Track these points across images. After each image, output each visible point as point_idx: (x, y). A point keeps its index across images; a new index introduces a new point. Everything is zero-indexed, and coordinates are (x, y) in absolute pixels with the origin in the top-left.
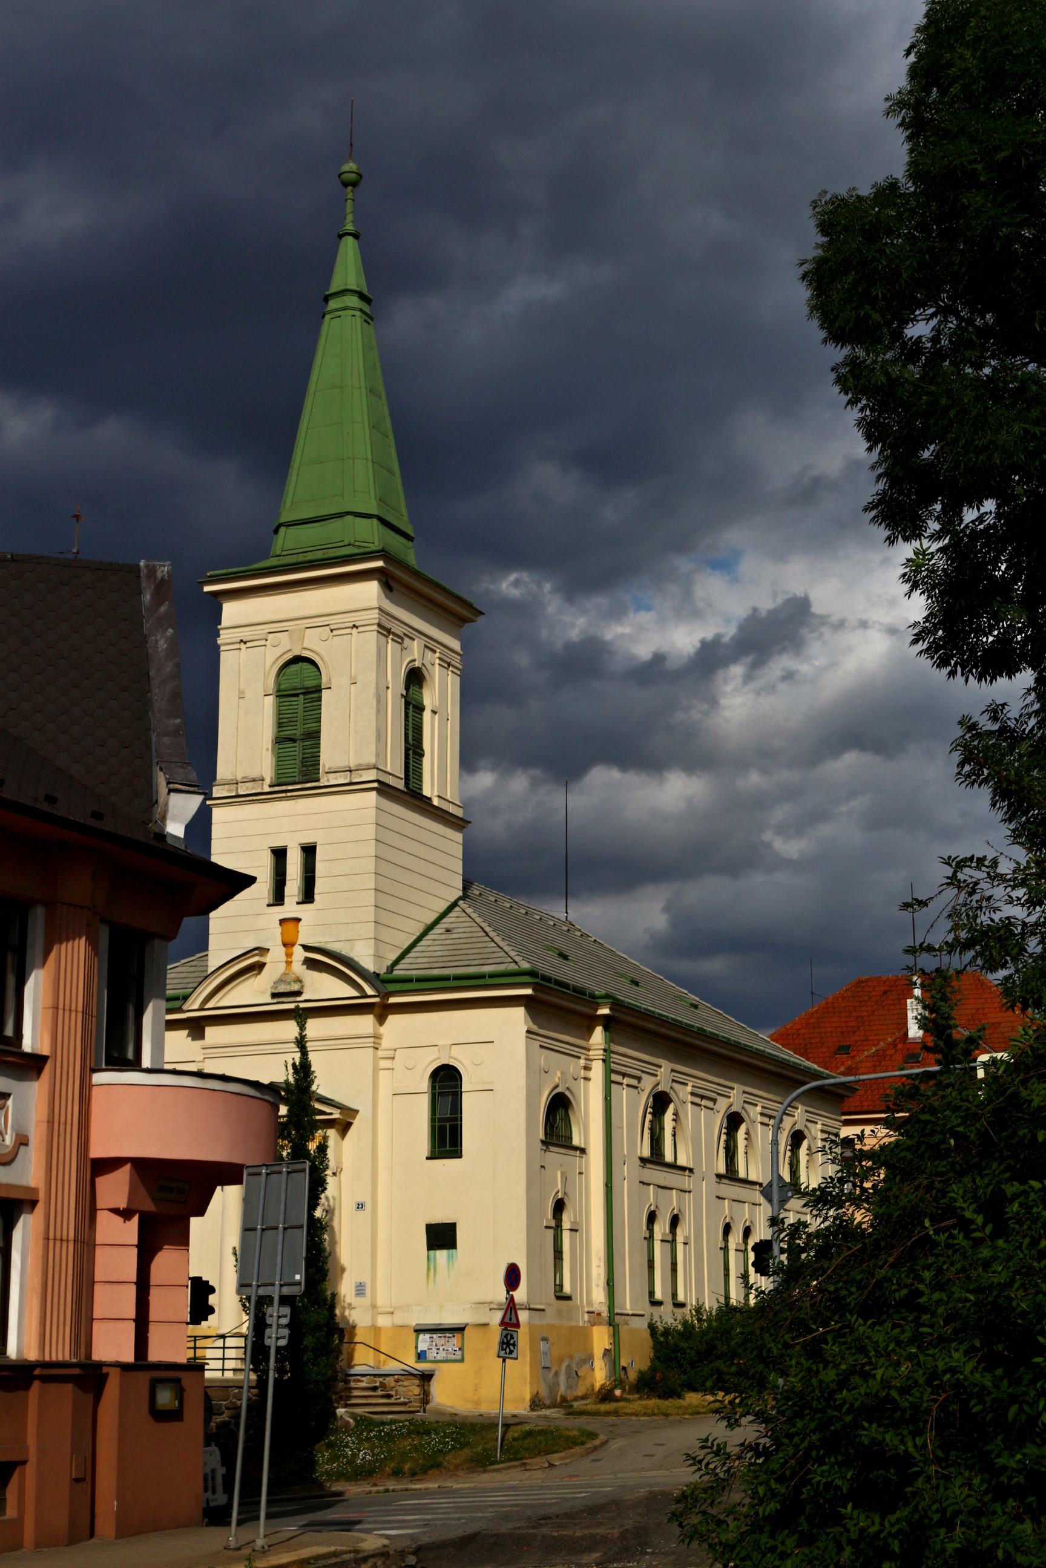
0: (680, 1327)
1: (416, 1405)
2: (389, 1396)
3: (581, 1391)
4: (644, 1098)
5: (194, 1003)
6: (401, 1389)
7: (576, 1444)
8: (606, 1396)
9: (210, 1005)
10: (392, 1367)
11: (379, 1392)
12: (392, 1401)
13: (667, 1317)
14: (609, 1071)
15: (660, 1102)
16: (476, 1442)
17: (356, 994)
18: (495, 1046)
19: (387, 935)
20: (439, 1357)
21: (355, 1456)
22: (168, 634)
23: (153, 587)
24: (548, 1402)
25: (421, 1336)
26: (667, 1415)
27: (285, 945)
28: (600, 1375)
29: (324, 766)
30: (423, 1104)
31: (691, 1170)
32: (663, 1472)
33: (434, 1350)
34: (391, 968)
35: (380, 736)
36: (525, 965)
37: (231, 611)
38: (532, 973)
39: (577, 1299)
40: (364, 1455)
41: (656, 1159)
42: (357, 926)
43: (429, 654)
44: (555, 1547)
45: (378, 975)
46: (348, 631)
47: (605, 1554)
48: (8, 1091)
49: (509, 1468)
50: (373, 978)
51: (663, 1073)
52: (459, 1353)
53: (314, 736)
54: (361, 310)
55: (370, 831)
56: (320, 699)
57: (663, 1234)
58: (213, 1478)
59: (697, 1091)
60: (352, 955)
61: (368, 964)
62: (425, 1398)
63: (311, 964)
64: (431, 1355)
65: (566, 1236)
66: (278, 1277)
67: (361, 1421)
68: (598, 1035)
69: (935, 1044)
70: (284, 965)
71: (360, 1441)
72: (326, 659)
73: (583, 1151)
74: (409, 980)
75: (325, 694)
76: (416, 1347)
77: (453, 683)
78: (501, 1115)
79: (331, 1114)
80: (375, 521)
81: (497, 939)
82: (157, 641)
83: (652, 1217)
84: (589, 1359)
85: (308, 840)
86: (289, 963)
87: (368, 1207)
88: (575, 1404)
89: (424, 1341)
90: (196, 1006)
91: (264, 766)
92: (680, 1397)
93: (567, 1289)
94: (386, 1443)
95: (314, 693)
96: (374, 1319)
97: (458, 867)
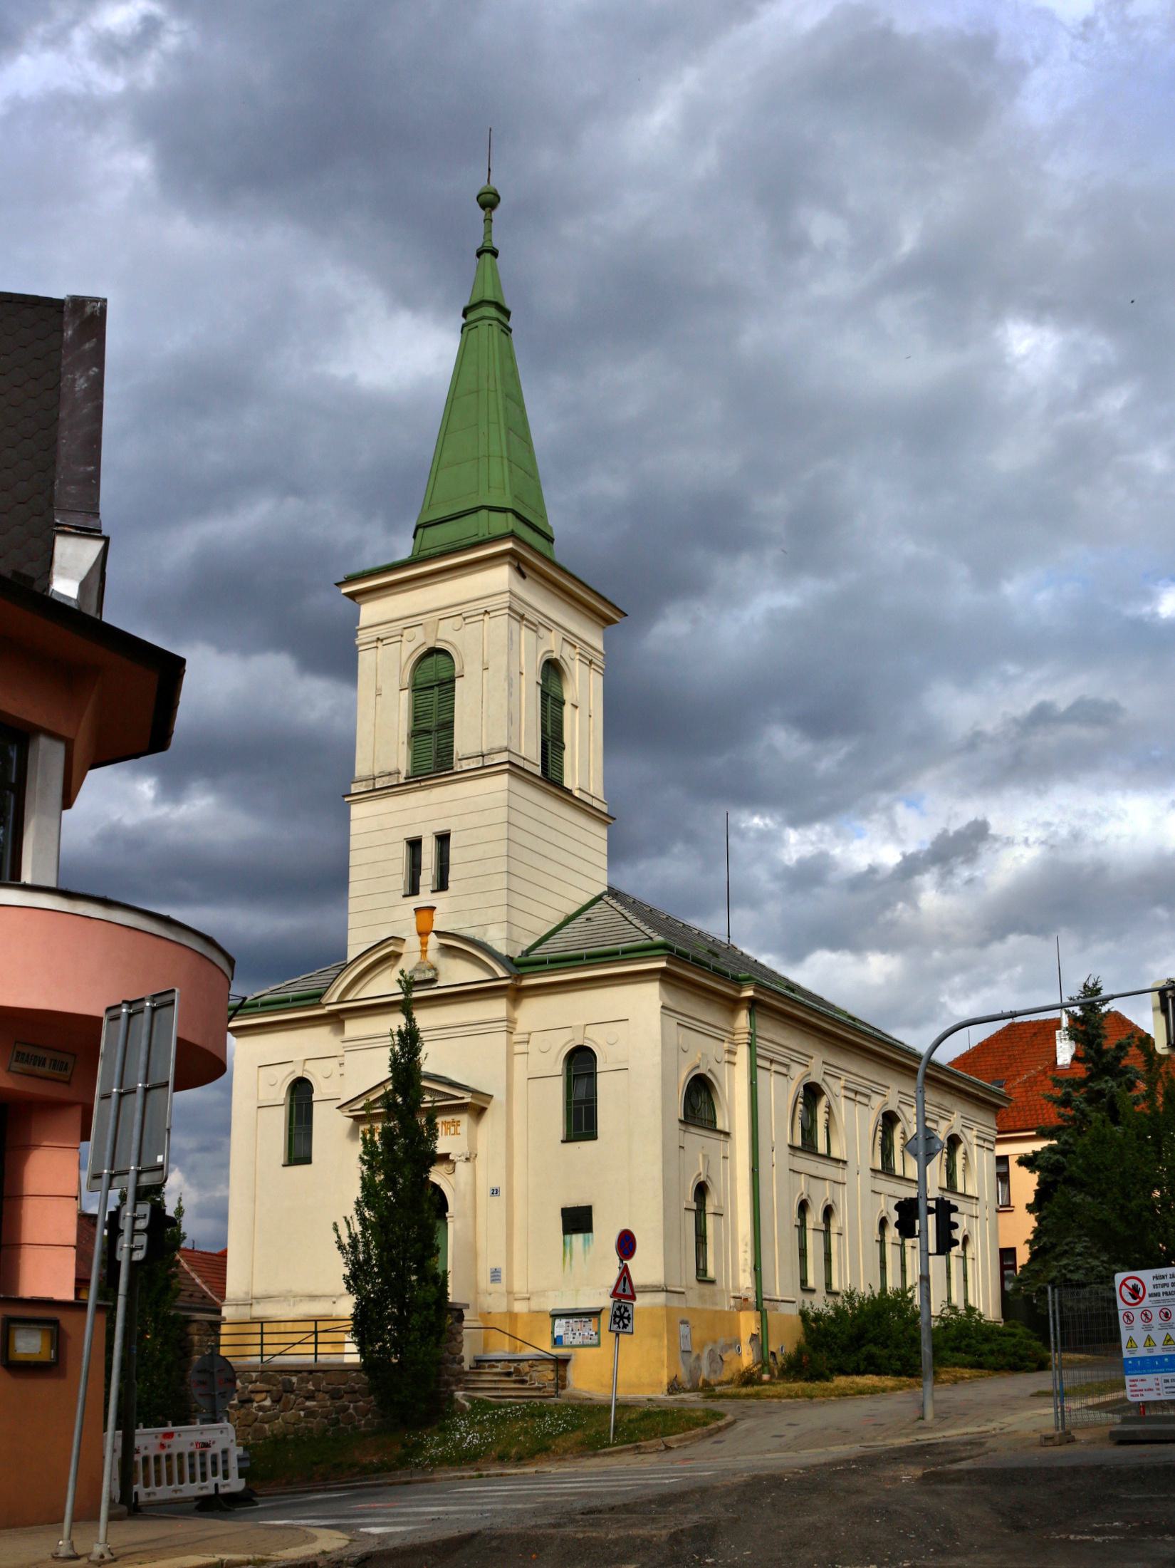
0: (832, 1313)
1: (551, 1389)
2: (523, 1382)
3: (726, 1376)
4: (793, 1088)
6: (534, 1374)
7: (697, 1425)
8: (748, 1379)
9: (350, 997)
10: (528, 1352)
11: (514, 1378)
12: (526, 1386)
13: (819, 1303)
14: (753, 1056)
15: (812, 1093)
16: (639, 1425)
18: (633, 1024)
19: (518, 918)
20: (575, 1342)
21: (463, 1439)
22: (91, 373)
23: (78, 322)
24: (688, 1386)
25: (557, 1322)
26: (811, 1397)
27: (420, 934)
28: (747, 1358)
30: (558, 1086)
31: (845, 1162)
32: (791, 1454)
33: (571, 1335)
34: (526, 953)
35: (511, 719)
36: (659, 939)
38: (665, 949)
39: (721, 1283)
40: (473, 1439)
41: (808, 1145)
43: (568, 648)
45: (512, 959)
46: (481, 617)
51: (817, 1064)
52: (595, 1337)
53: (448, 726)
55: (502, 815)
56: (453, 689)
57: (816, 1223)
58: (225, 1462)
59: (850, 1085)
60: (485, 940)
61: (501, 948)
62: (561, 1382)
63: (447, 950)
64: (567, 1341)
65: (710, 1221)
66: (134, 1159)
68: (743, 1019)
69: (1087, 1053)
70: (419, 954)
71: (472, 1425)
72: (460, 648)
73: (727, 1134)
74: (543, 962)
75: (458, 683)
76: (553, 1333)
77: (596, 682)
78: (636, 1096)
80: (510, 515)
81: (634, 922)
82: (74, 380)
83: (803, 1207)
84: (735, 1345)
85: (441, 827)
86: (424, 952)
87: (503, 1192)
88: (718, 1389)
89: (560, 1326)
90: (334, 999)
91: (399, 758)
93: (711, 1272)
94: (497, 1426)
95: (447, 685)
96: (509, 1304)
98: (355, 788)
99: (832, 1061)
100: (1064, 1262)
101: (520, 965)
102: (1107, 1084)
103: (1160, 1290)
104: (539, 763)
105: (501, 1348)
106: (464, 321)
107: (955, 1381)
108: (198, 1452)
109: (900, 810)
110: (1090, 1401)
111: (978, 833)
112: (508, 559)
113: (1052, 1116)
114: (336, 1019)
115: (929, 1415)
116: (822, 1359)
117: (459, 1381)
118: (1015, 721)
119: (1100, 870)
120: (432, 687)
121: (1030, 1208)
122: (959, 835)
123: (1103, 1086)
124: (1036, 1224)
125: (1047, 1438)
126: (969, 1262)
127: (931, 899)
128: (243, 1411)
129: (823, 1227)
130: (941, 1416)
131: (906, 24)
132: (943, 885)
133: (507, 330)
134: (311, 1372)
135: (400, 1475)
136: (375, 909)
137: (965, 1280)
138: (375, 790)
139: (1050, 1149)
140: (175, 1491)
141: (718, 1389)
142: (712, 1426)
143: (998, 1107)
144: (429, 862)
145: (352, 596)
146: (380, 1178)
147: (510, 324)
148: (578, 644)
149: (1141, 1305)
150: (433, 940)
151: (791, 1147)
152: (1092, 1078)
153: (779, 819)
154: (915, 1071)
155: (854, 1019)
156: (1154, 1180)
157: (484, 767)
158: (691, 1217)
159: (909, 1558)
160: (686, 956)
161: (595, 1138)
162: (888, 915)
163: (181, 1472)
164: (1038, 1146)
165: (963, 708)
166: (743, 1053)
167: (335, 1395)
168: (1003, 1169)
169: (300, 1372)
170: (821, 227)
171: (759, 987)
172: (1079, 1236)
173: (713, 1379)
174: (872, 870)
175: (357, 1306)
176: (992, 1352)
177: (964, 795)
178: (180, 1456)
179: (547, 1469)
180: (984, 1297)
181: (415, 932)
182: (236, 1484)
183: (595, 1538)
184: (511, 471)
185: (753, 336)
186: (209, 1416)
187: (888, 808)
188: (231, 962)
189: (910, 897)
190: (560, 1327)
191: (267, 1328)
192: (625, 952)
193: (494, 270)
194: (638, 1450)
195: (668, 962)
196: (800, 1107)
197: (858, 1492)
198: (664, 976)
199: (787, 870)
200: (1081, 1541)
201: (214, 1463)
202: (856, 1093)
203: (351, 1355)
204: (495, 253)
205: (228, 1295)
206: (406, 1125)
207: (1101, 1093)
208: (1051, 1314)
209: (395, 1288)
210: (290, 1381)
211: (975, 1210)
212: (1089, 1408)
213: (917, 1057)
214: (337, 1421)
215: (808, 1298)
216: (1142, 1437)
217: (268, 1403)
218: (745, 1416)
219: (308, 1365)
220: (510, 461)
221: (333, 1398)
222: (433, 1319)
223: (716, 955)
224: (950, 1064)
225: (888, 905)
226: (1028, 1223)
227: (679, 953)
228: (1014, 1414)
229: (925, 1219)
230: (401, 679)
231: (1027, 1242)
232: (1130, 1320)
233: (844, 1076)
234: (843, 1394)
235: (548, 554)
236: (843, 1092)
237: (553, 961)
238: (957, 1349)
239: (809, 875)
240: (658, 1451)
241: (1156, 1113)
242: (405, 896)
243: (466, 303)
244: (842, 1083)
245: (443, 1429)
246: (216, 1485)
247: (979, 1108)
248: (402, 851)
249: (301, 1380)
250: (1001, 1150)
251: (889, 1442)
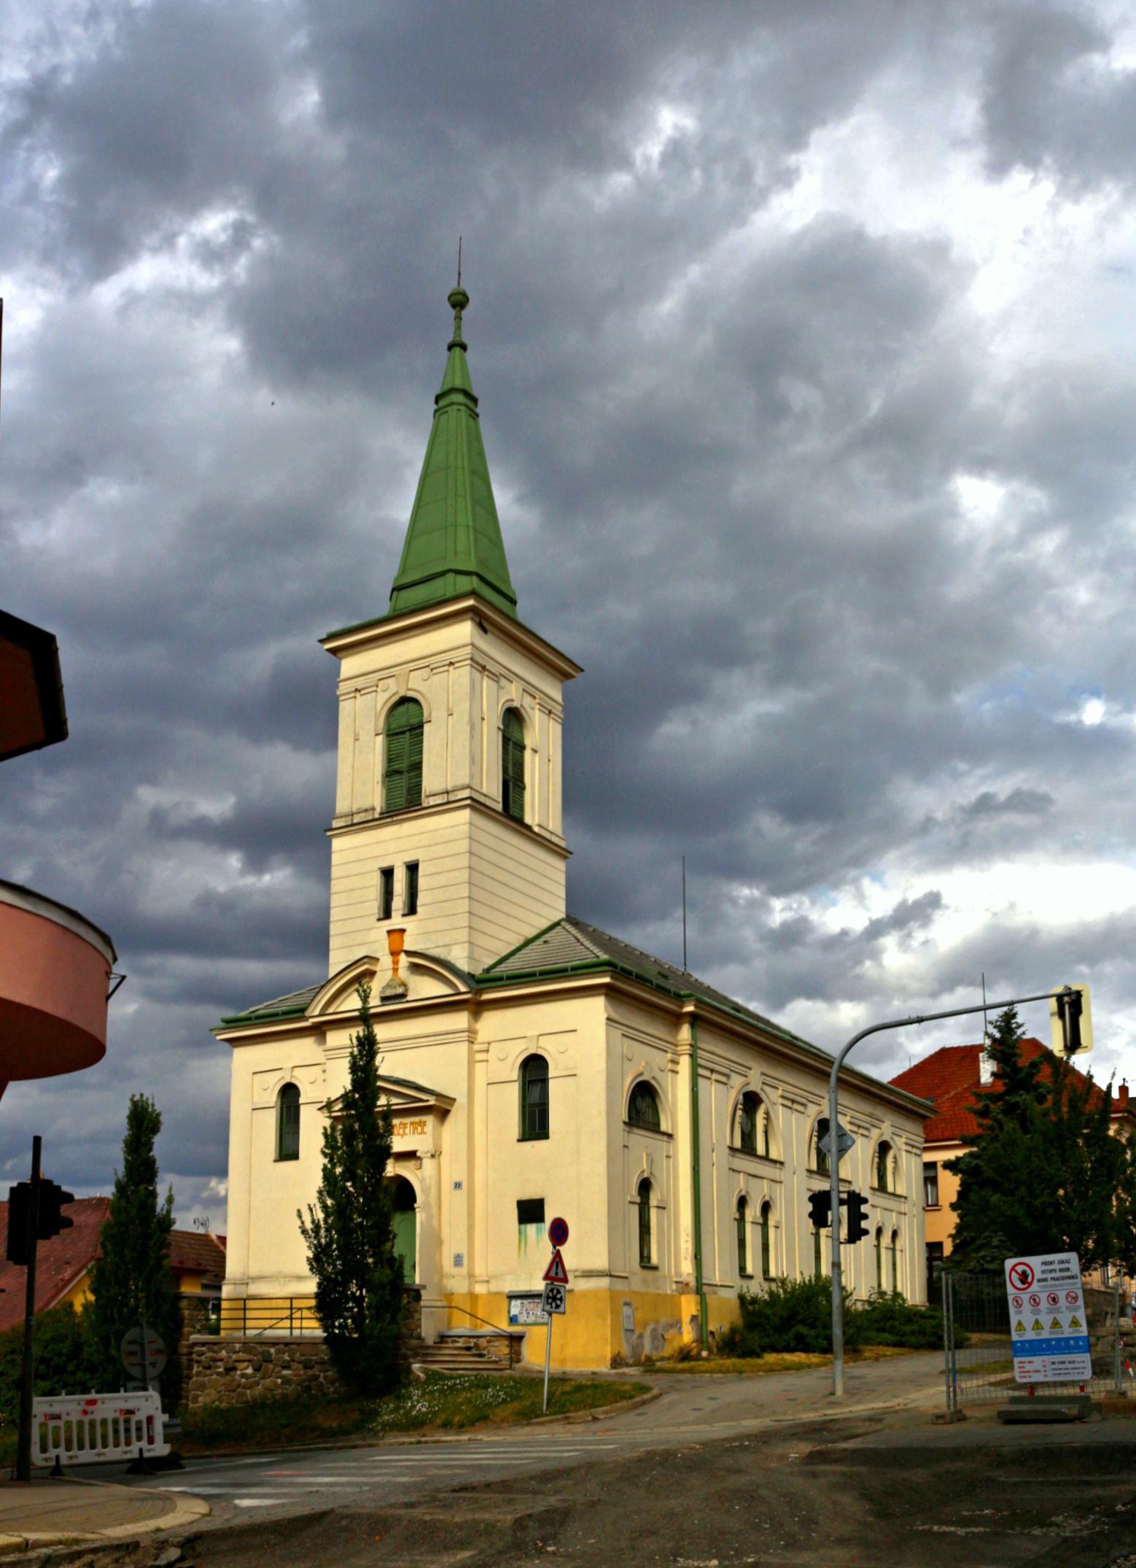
0: (766, 1297)
1: (506, 1363)
2: (481, 1355)
4: (733, 1095)
9: (330, 1010)
10: (487, 1330)
11: (474, 1351)
13: (757, 1288)
14: (695, 1066)
15: (751, 1101)
16: (573, 1396)
17: (450, 991)
18: (580, 1036)
21: (413, 1407)
24: (631, 1361)
25: (513, 1302)
26: (741, 1372)
30: (513, 1092)
31: (782, 1163)
32: (705, 1427)
34: (487, 971)
35: (474, 760)
38: (610, 967)
39: (664, 1269)
40: (422, 1407)
41: (747, 1147)
43: (528, 700)
44: (430, 1537)
45: (473, 976)
47: (482, 1551)
49: (551, 1422)
50: (468, 978)
51: (756, 1075)
53: (417, 767)
54: (467, 406)
55: (464, 845)
56: (422, 734)
57: (754, 1217)
61: (463, 965)
62: (516, 1356)
63: (415, 968)
64: (522, 1319)
65: (654, 1213)
67: (434, 1377)
68: (685, 1032)
71: (423, 1395)
72: (428, 696)
73: (670, 1136)
74: (500, 979)
75: (426, 727)
83: (742, 1202)
84: (677, 1324)
85: (410, 858)
86: (395, 970)
87: (465, 1185)
90: (317, 1012)
91: (376, 798)
92: (759, 1356)
93: (654, 1259)
94: (446, 1396)
95: (416, 730)
96: (471, 1285)
97: (562, 892)
98: (335, 824)
99: (770, 1072)
100: (982, 1253)
101: (479, 982)
102: (1022, 1097)
103: (1049, 1276)
104: (500, 799)
105: (462, 1326)
106: (435, 407)
107: (877, 1359)
108: (122, 1419)
109: (866, 883)
110: (993, 1379)
111: (933, 901)
112: (470, 615)
113: (974, 1126)
114: (319, 1031)
115: (839, 1392)
116: (755, 1339)
117: (417, 1355)
118: (962, 809)
119: (1034, 933)
121: (954, 1207)
122: (917, 904)
123: (1018, 1099)
124: (958, 1221)
125: (939, 1417)
126: (898, 1254)
127: (895, 959)
128: (228, 1378)
129: (761, 1221)
130: (849, 1392)
131: (875, 228)
132: (904, 945)
133: (475, 416)
134: (287, 1344)
135: (355, 1439)
136: (355, 932)
137: (894, 1269)
138: (353, 825)
139: (971, 1155)
140: (99, 1455)
141: (658, 1364)
142: (637, 1399)
143: (923, 1117)
144: (400, 889)
145: (334, 651)
146: (338, 1170)
147: (478, 410)
148: (538, 694)
149: (1030, 1290)
150: (404, 960)
151: (731, 1148)
152: (1007, 1092)
153: (764, 887)
154: (828, 1075)
155: (796, 1038)
156: (1056, 1180)
157: (448, 803)
158: (635, 1210)
159: (756, 1552)
160: (630, 973)
162: (858, 970)
163: (104, 1437)
164: (960, 1153)
165: (924, 799)
166: (685, 1064)
167: (308, 1365)
168: (931, 1174)
170: (799, 394)
171: (699, 1003)
172: (995, 1232)
173: (655, 1356)
174: (844, 933)
175: (319, 1285)
176: (913, 1333)
177: (919, 871)
178: (104, 1422)
179: (480, 1437)
180: (911, 1287)
181: (387, 952)
182: (161, 1449)
183: (441, 1521)
184: (476, 540)
185: (743, 487)
186: (141, 1384)
187: (856, 881)
188: (106, 939)
189: (875, 955)
190: (516, 1307)
191: (250, 1304)
192: (574, 969)
193: (463, 362)
194: (568, 1420)
195: (612, 977)
196: (739, 1113)
197: (739, 1471)
198: (608, 990)
199: (772, 931)
200: (945, 1534)
201: (139, 1429)
202: (793, 1101)
203: (312, 1328)
204: (464, 347)
205: (227, 1275)
206: (364, 1124)
207: (1016, 1105)
208: (965, 1303)
209: (354, 1270)
210: (269, 1353)
211: (904, 1208)
212: (991, 1384)
213: (828, 1061)
214: (309, 1388)
215: (745, 1283)
216: (1029, 1417)
217: (250, 1371)
218: (672, 1389)
219: (284, 1338)
220: (475, 530)
221: (305, 1368)
222: (388, 1298)
223: (665, 977)
224: (890, 1083)
225: (859, 962)
226: (952, 1219)
227: (623, 970)
228: (912, 1390)
229: (835, 1209)
230: (376, 725)
231: (950, 1236)
232: (1019, 1305)
233: (781, 1086)
234: (771, 1370)
235: (511, 614)
236: (781, 1101)
237: (509, 978)
238: (883, 1330)
239: (792, 935)
240: (585, 1422)
241: (1061, 1119)
242: (379, 920)
243: (438, 391)
244: (780, 1092)
245: (398, 1398)
246: (141, 1450)
247: (908, 1118)
248: (377, 879)
249: (278, 1352)
250: (929, 1157)
251: (799, 1416)
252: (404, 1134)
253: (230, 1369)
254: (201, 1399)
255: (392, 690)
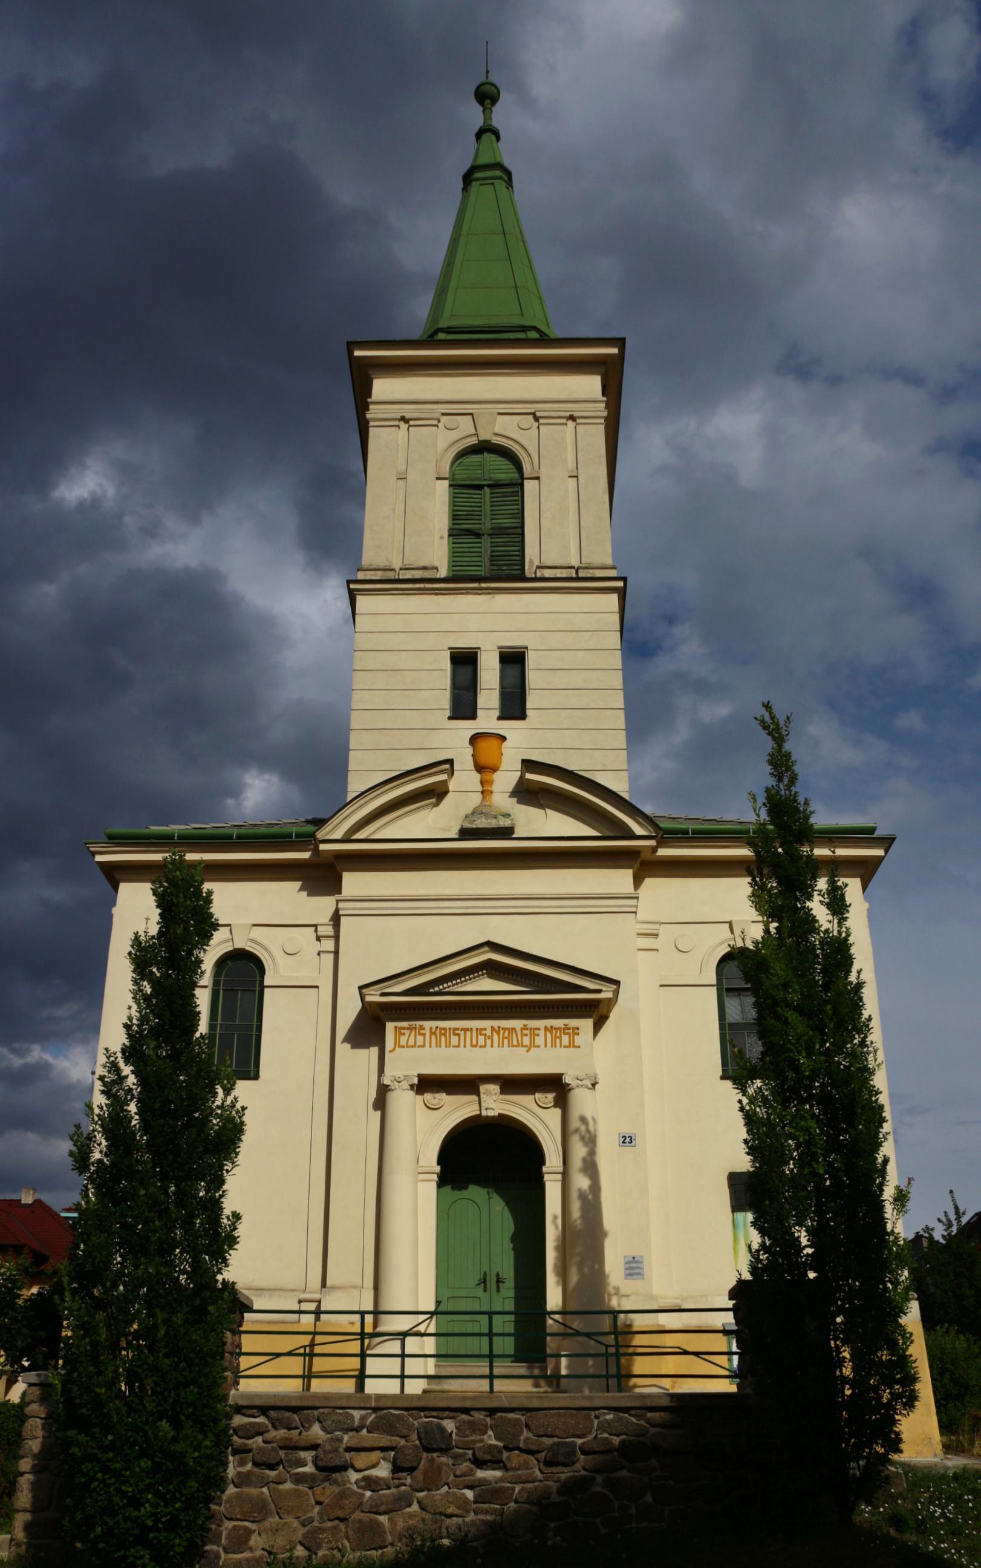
5: (336, 829)
29: (531, 561)
37: (383, 387)
42: (598, 753)
48: (98, 868)
70: (480, 796)
75: (529, 486)
79: (599, 991)
85: (513, 641)
86: (486, 792)
90: (338, 834)
91: (436, 552)
95: (512, 489)
120: (480, 487)
161: (256, 1077)
169: (466, 1411)
210: (442, 1430)
217: (383, 1471)
252: (533, 1045)
253: (330, 1469)
254: (255, 1540)
255: (462, 432)
